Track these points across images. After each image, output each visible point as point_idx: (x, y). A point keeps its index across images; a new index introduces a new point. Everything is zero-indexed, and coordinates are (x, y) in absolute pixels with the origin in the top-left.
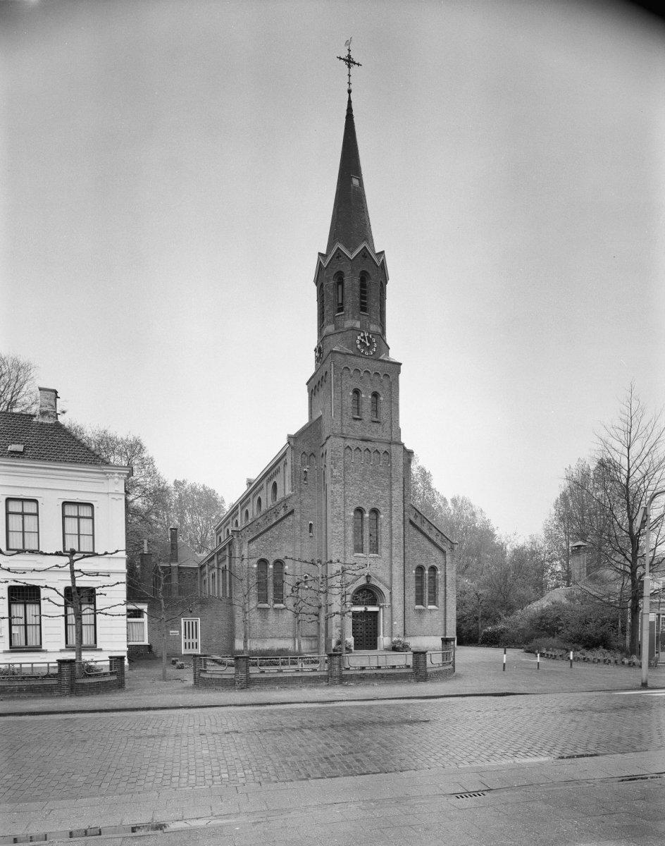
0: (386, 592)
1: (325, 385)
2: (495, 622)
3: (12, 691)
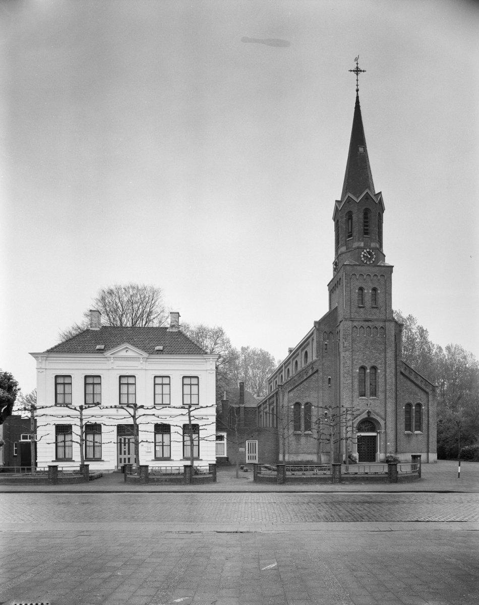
0: (382, 422)
1: (340, 287)
2: (472, 443)
3: (162, 481)
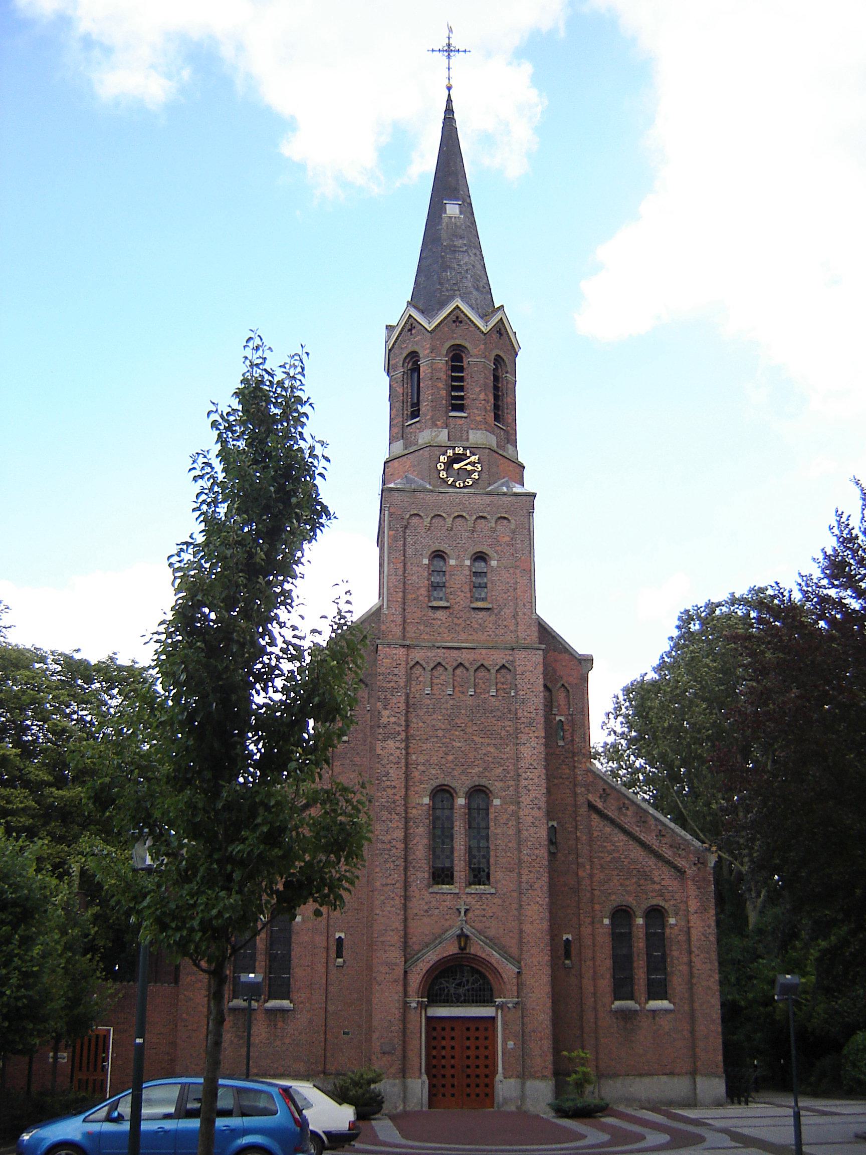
0: (508, 970)
